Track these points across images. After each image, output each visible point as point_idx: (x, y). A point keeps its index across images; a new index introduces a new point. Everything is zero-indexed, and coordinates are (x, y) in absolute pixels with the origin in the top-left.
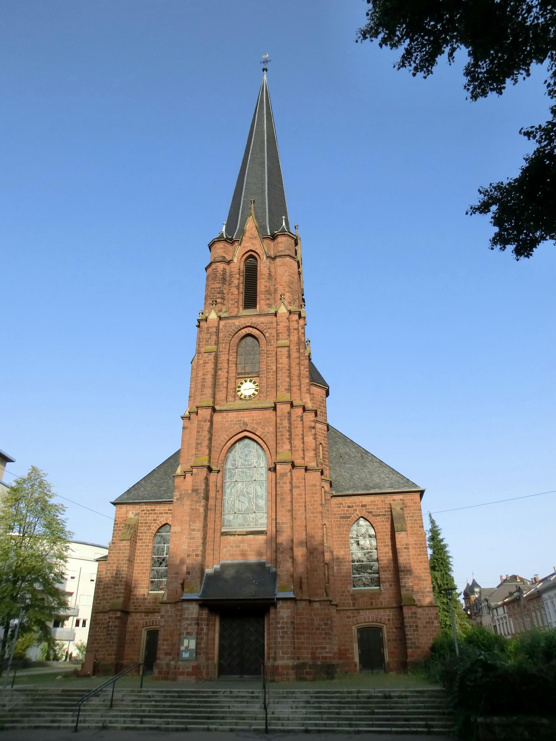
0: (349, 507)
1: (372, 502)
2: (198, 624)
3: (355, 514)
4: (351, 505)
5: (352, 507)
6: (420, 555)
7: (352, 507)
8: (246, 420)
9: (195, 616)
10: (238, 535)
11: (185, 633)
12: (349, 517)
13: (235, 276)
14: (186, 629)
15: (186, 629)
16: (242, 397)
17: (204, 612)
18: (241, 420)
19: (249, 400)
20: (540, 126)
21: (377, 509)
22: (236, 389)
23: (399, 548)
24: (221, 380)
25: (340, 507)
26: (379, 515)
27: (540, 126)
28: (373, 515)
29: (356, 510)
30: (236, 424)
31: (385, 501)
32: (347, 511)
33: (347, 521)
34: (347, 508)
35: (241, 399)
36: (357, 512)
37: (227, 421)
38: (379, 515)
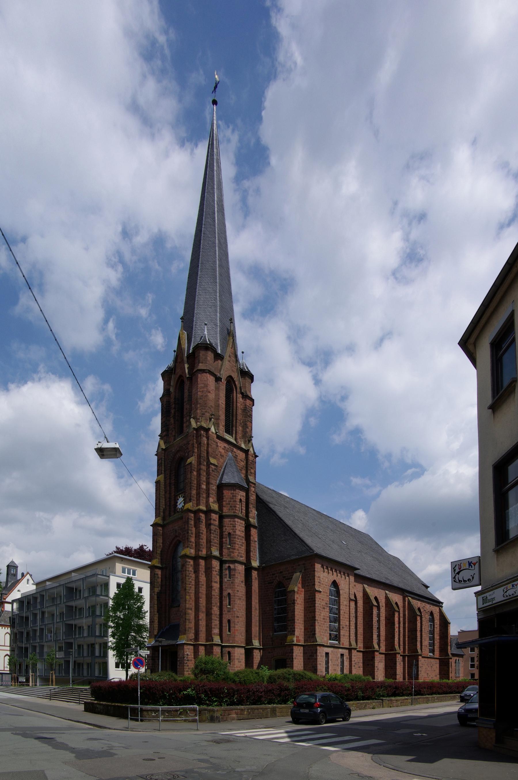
0: (273, 574)
29: (276, 577)
32: (272, 577)
36: (277, 578)
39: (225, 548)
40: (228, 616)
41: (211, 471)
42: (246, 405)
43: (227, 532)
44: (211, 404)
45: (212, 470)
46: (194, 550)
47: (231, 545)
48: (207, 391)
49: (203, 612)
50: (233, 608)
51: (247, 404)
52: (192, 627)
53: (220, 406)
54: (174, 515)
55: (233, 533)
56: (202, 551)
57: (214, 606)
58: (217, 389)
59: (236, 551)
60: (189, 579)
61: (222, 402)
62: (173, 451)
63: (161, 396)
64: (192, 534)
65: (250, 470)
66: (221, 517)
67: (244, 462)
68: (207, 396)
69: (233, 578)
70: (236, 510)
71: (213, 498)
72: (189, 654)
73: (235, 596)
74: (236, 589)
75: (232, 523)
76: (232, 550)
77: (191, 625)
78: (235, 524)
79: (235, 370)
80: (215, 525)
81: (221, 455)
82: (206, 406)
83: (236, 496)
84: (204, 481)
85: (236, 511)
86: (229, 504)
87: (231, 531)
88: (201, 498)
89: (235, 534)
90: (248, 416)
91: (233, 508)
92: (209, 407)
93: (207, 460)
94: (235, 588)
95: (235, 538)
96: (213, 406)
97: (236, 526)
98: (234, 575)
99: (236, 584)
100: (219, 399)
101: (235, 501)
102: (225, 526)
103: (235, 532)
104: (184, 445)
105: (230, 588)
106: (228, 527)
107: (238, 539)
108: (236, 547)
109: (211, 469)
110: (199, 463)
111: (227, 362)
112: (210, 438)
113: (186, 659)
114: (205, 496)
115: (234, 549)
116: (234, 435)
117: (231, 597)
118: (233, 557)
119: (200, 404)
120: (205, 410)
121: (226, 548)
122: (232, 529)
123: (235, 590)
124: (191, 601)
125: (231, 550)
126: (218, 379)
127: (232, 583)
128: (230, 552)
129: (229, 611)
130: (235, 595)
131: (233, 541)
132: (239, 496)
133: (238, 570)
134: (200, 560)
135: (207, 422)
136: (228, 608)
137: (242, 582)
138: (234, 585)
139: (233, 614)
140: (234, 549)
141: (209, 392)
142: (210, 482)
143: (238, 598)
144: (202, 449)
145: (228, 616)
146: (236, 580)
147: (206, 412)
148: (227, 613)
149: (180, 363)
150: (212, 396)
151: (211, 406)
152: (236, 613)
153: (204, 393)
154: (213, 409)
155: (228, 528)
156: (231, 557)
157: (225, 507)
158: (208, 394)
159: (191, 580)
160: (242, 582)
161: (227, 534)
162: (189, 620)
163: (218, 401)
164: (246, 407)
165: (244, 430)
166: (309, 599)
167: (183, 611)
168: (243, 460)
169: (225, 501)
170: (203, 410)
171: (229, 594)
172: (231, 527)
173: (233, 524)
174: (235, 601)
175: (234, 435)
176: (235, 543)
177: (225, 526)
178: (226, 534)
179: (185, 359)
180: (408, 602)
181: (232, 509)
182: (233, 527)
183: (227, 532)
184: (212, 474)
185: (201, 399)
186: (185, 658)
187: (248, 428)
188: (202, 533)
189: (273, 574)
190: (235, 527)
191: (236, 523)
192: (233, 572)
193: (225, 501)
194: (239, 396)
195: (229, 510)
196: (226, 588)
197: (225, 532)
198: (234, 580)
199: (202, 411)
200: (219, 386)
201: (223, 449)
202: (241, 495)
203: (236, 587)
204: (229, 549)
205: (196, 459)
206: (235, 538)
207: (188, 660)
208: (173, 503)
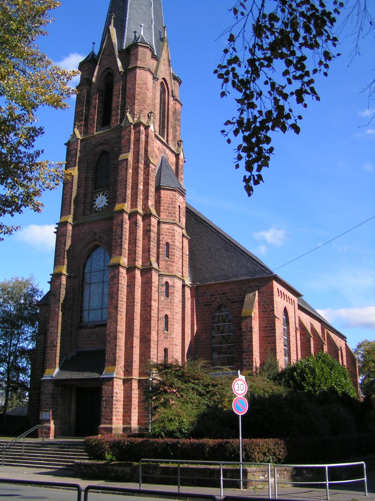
0: (211, 295)
1: (231, 289)
2: (53, 398)
3: (216, 302)
4: (213, 294)
5: (214, 295)
6: (269, 337)
7: (214, 295)
8: (96, 230)
9: (51, 392)
10: (90, 328)
11: (45, 404)
12: (211, 305)
13: (94, 97)
14: (45, 401)
15: (45, 401)
16: (96, 210)
17: (59, 388)
18: (91, 231)
19: (102, 211)
20: (25, 207)
21: (235, 296)
22: (92, 203)
23: (135, 332)
24: (80, 197)
25: (204, 296)
26: (236, 302)
27: (25, 207)
28: (231, 302)
29: (217, 298)
30: (88, 235)
31: (242, 288)
32: (210, 299)
33: (209, 308)
34: (210, 297)
35: (96, 211)
36: (218, 300)
37: (82, 233)
38: (236, 302)
39: (162, 260)
40: (164, 343)
41: (150, 171)
42: (176, 109)
43: (165, 241)
44: (149, 101)
45: (152, 171)
46: (127, 260)
47: (170, 257)
48: (146, 88)
49: (137, 337)
50: (171, 334)
51: (177, 108)
52: (122, 356)
53: (156, 105)
54: (90, 214)
55: (172, 243)
56: (138, 261)
57: (153, 330)
58: (154, 88)
59: (175, 264)
60: (121, 294)
61: (158, 101)
62: (93, 143)
63: (78, 85)
64: (126, 239)
65: (181, 175)
66: (159, 223)
67: (174, 166)
68: (146, 93)
69: (171, 296)
70: (175, 217)
71: (152, 201)
72: (118, 391)
73: (173, 318)
74: (175, 311)
75: (170, 231)
76: (170, 263)
77: (121, 353)
78: (174, 233)
79: (168, 74)
80: (154, 232)
81: (156, 155)
82: (145, 103)
83: (175, 202)
84: (141, 181)
85: (176, 219)
86: (168, 210)
87: (169, 241)
88: (138, 199)
89: (174, 245)
90: (177, 119)
91: (172, 215)
92: (147, 105)
93: (146, 159)
94: (173, 308)
95: (174, 249)
96: (151, 104)
97: (176, 235)
98: (173, 293)
99: (175, 305)
100: (155, 98)
101: (175, 208)
102: (163, 235)
103: (174, 242)
104: (112, 139)
105: (168, 309)
106: (166, 235)
107: (177, 250)
108: (175, 260)
109: (150, 169)
110: (136, 161)
111: (163, 65)
112: (149, 136)
113: (115, 399)
114: (142, 198)
115: (173, 262)
116: (165, 137)
117: (169, 320)
118: (172, 272)
119: (137, 99)
120: (143, 107)
121: (163, 259)
122: (170, 239)
123: (174, 311)
124: (122, 322)
125: (169, 263)
126: (155, 78)
127: (171, 302)
128: (168, 265)
129: (165, 338)
130: (173, 318)
131: (172, 252)
132: (178, 202)
133: (177, 287)
134: (274, 281)
135: (145, 119)
136: (165, 333)
137: (180, 301)
138: (173, 306)
139: (170, 341)
140: (173, 262)
141: (148, 90)
142: (149, 182)
143: (176, 321)
144: (140, 146)
145: (164, 343)
146: (175, 300)
147: (145, 109)
148: (163, 339)
149: (108, 56)
150: (150, 94)
151: (149, 104)
152: (175, 340)
153: (143, 90)
154: (150, 107)
155: (166, 237)
156: (169, 272)
157: (163, 212)
158: (147, 92)
159: (123, 295)
160: (180, 301)
161: (165, 243)
162: (120, 346)
163: (154, 100)
164: (176, 111)
165: (174, 133)
166: (265, 327)
167: (112, 334)
168: (173, 164)
169: (163, 206)
170: (141, 107)
171: (166, 316)
172: (169, 236)
173: (172, 233)
174: (173, 325)
175: (165, 137)
176: (174, 255)
177: (163, 235)
178: (163, 244)
179: (117, 54)
180: (327, 335)
181: (171, 216)
182: (172, 236)
183: (164, 242)
184: (151, 175)
185: (139, 95)
186: (114, 398)
187: (177, 132)
188: (139, 240)
189: (211, 295)
190: (174, 236)
191: (175, 232)
192: (171, 289)
193: (163, 206)
194: (171, 98)
195: (168, 216)
196: (162, 308)
197: (162, 241)
198: (173, 299)
199: (140, 107)
200: (156, 86)
201: (157, 149)
202: (180, 201)
203: (175, 308)
204: (167, 262)
205: (132, 156)
206: (174, 249)
207: (117, 401)
208: (89, 200)
